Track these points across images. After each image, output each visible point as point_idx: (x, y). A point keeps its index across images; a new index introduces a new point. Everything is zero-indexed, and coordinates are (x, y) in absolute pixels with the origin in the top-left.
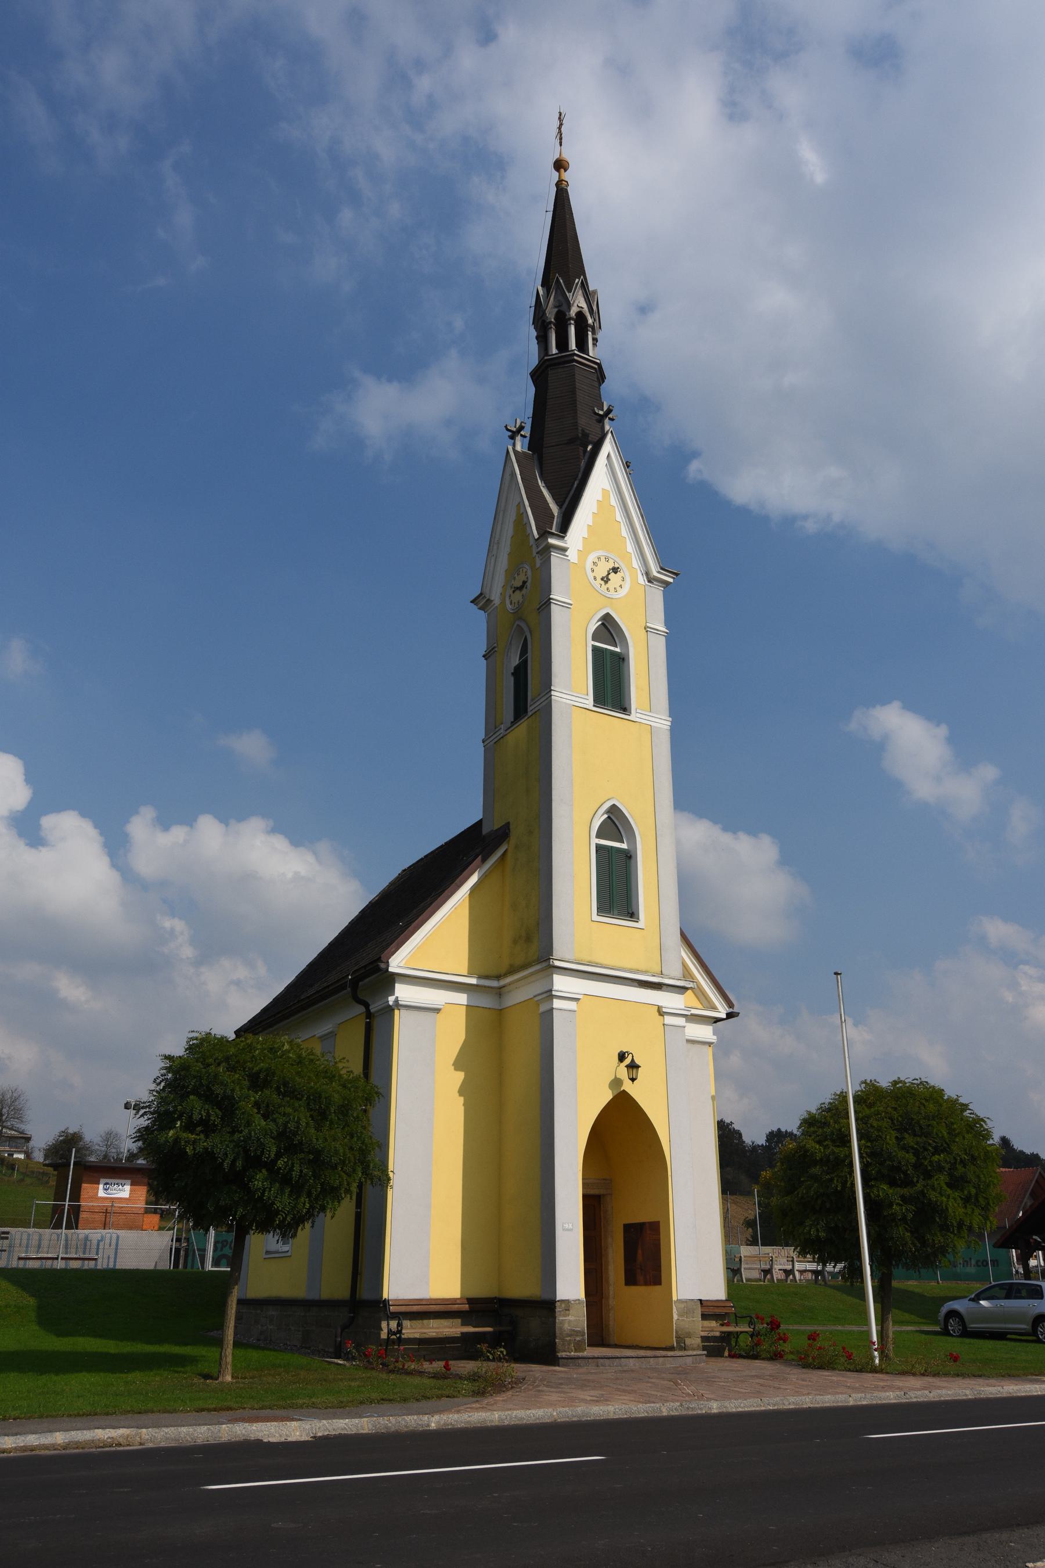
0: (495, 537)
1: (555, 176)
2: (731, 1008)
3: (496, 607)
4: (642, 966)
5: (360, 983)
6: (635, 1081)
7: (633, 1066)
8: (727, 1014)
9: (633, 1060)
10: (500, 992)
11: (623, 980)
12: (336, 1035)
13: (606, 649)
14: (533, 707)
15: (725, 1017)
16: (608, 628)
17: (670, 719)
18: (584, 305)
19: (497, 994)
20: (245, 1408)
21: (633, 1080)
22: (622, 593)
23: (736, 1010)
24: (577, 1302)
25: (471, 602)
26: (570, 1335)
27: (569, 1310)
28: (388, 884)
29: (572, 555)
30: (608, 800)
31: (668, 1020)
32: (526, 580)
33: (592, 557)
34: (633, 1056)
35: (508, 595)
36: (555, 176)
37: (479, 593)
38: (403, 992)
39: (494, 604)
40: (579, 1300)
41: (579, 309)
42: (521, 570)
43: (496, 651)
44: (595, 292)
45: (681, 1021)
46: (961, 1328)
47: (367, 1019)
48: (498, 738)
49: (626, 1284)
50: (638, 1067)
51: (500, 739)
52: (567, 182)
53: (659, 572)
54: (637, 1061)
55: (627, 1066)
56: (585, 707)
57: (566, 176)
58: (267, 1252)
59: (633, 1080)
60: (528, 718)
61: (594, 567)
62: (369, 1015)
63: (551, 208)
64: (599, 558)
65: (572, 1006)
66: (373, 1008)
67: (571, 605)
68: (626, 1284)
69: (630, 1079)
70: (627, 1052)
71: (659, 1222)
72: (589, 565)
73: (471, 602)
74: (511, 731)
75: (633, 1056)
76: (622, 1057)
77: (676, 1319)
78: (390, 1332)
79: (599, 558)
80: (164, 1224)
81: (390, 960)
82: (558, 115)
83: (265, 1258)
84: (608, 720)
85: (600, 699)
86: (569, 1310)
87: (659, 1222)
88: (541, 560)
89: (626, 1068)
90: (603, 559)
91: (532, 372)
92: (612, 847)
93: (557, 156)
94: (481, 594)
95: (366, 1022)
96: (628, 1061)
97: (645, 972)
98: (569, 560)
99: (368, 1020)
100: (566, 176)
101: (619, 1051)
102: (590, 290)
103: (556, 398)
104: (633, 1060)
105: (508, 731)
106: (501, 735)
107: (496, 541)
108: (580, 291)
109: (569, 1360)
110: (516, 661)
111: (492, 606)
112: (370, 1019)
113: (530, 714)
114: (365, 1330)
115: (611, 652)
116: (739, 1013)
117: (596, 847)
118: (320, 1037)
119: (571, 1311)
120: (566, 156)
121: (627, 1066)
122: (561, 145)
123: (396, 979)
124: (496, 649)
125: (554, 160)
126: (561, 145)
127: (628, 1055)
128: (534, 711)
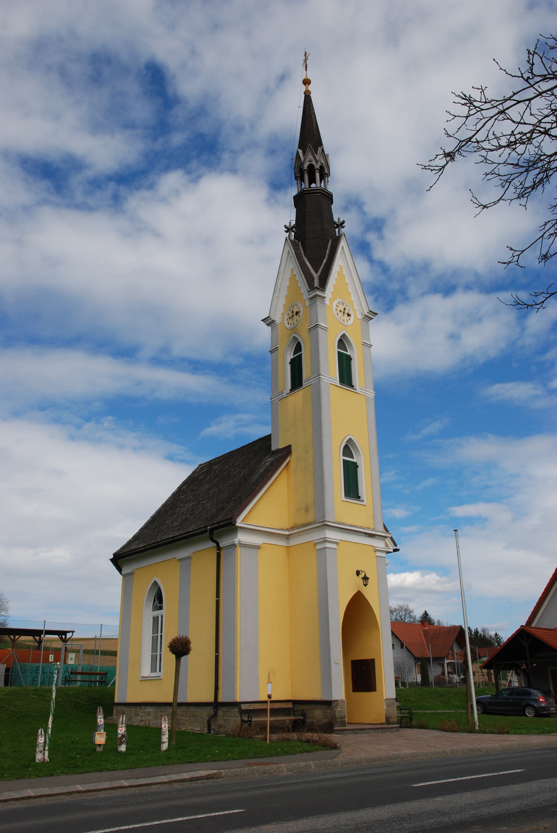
0: (277, 286)
1: (303, 88)
2: (395, 546)
3: (277, 324)
4: (365, 525)
5: (215, 531)
6: (367, 586)
7: (365, 578)
8: (394, 550)
9: (365, 575)
10: (288, 537)
11: (336, 528)
12: (191, 558)
13: (343, 353)
14: (305, 384)
15: (392, 551)
16: (342, 342)
17: (374, 392)
18: (323, 162)
19: (286, 538)
20: (269, 773)
21: (366, 585)
22: (350, 322)
23: (398, 548)
24: (342, 701)
25: (262, 320)
26: (340, 718)
27: (338, 705)
28: (192, 472)
29: (327, 301)
30: (348, 435)
31: (378, 554)
32: (298, 311)
33: (335, 303)
34: (365, 573)
35: (286, 320)
36: (303, 88)
37: (268, 316)
38: (242, 537)
39: (276, 323)
40: (342, 700)
41: (321, 164)
42: (295, 306)
43: (278, 349)
44: (328, 155)
45: (384, 555)
46: (533, 709)
47: (217, 551)
48: (282, 398)
49: (354, 691)
50: (368, 578)
51: (283, 398)
52: (310, 92)
53: (368, 313)
54: (368, 576)
55: (363, 578)
56: (336, 385)
57: (310, 88)
58: (142, 677)
59: (366, 585)
60: (303, 388)
61: (337, 308)
62: (219, 548)
63: (302, 105)
64: (339, 303)
65: (334, 546)
66: (222, 545)
67: (327, 328)
68: (354, 691)
69: (364, 585)
70: (361, 571)
71: (374, 659)
72: (334, 307)
73: (262, 320)
74: (291, 394)
75: (365, 573)
76: (358, 573)
77: (385, 708)
78: (242, 721)
79: (339, 303)
80: (100, 663)
81: (237, 520)
82: (304, 54)
83: (141, 680)
84: (344, 392)
85: (342, 381)
86: (338, 705)
87: (374, 659)
88: (310, 302)
89: (362, 579)
90: (341, 303)
91: (295, 196)
92: (349, 461)
93: (304, 77)
94: (269, 317)
95: (217, 553)
96: (362, 575)
97: (368, 528)
98: (325, 304)
99: (218, 551)
100: (310, 88)
101: (356, 570)
102: (325, 153)
103: (310, 212)
104: (365, 575)
105: (288, 395)
106: (284, 397)
107: (278, 288)
108: (310, 153)
109: (340, 731)
110: (290, 356)
111: (274, 324)
112: (219, 550)
113: (304, 386)
114: (224, 718)
115: (345, 355)
116: (399, 549)
117: (343, 461)
118: (179, 560)
119: (339, 706)
120: (309, 77)
121: (363, 578)
122: (306, 71)
123: (238, 530)
124: (278, 348)
125: (303, 79)
126: (306, 71)
127: (362, 572)
128: (307, 385)
